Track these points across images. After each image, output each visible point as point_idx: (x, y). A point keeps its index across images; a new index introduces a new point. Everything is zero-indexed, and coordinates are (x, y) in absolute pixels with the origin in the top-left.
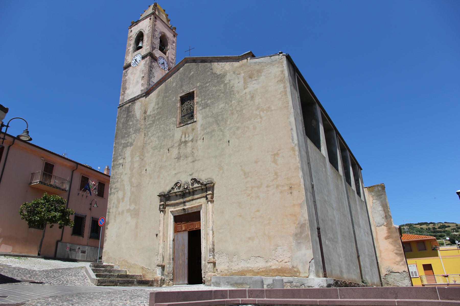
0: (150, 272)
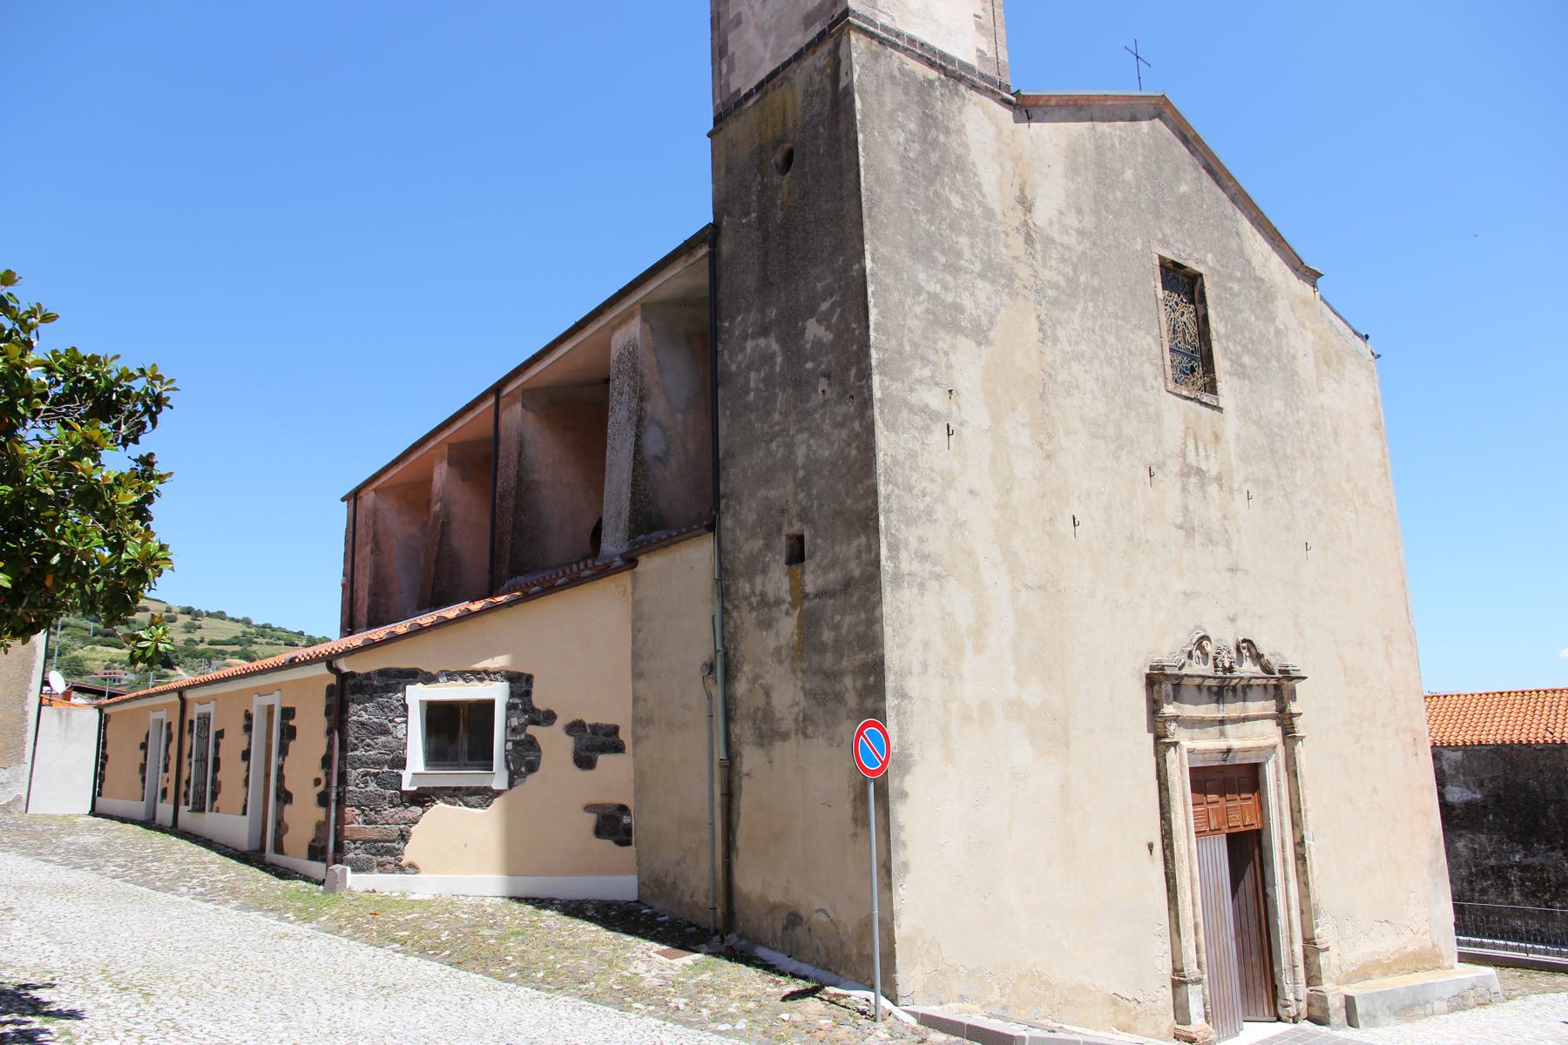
0: (1145, 1011)
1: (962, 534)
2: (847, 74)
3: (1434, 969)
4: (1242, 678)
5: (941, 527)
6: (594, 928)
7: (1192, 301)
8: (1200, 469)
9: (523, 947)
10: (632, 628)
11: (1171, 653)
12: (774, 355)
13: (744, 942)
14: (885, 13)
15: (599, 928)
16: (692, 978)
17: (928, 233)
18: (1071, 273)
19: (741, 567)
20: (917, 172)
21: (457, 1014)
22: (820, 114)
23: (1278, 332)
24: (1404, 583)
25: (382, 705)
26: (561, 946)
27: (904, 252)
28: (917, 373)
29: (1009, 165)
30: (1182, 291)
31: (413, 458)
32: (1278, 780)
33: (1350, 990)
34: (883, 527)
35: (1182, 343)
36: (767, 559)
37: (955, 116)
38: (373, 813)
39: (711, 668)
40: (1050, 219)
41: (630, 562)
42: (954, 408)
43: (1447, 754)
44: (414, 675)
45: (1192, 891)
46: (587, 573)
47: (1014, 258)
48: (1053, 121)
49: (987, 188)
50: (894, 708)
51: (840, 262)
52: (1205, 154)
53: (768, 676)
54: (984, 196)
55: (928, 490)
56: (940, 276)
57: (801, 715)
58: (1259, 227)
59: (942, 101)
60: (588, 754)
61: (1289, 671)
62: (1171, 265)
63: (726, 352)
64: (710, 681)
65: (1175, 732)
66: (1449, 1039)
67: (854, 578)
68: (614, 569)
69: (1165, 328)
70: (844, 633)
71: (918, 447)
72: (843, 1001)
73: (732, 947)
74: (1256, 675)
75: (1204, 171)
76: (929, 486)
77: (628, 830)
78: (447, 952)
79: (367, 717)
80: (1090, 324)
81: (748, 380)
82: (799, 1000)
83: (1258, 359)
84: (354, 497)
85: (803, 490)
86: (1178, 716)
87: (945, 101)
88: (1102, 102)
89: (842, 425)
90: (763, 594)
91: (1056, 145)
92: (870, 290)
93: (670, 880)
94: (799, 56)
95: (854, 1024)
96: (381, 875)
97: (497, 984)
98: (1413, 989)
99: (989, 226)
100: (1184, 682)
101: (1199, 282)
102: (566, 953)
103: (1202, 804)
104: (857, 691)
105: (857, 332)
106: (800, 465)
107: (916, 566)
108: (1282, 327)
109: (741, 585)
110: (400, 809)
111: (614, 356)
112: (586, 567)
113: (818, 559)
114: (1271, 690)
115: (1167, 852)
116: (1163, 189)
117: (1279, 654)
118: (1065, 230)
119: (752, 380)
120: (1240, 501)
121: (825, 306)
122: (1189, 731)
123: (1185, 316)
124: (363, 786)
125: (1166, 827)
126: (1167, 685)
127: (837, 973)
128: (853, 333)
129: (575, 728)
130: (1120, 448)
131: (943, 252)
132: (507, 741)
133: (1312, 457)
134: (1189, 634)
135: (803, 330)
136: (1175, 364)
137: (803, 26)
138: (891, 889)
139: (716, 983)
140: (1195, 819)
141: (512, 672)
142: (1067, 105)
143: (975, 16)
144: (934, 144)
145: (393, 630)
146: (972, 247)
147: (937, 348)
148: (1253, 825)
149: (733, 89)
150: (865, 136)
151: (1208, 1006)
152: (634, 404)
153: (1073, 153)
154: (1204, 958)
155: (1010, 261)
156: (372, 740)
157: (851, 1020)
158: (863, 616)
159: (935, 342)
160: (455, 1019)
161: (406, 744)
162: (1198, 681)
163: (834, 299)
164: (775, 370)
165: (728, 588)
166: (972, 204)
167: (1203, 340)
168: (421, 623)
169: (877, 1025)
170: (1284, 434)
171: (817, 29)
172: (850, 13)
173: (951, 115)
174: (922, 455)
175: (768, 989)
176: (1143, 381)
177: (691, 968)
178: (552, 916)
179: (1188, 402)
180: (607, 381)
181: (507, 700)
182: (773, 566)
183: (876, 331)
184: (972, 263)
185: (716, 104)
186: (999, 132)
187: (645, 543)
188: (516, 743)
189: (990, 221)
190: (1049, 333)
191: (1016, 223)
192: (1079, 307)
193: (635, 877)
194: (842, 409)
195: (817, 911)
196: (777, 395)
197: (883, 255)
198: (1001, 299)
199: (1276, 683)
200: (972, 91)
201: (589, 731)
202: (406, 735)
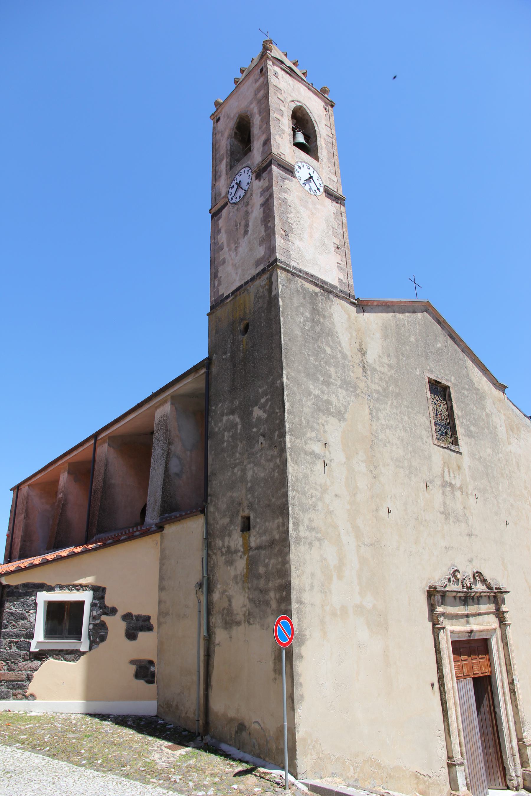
0: (434, 782)
1: (332, 517)
2: (275, 289)
4: (476, 592)
5: (321, 513)
6: (132, 732)
7: (445, 400)
9: (91, 744)
12: (237, 424)
13: (214, 740)
14: (295, 261)
15: (135, 732)
17: (314, 365)
18: (385, 386)
19: (218, 532)
21: (50, 788)
22: (262, 307)
23: (487, 415)
25: (23, 603)
26: (112, 743)
27: (302, 375)
28: (308, 435)
29: (354, 334)
30: (440, 395)
31: (50, 469)
32: (498, 647)
34: (291, 513)
35: (441, 420)
36: (231, 528)
37: (328, 309)
38: (13, 664)
39: (200, 585)
41: (160, 528)
42: (327, 452)
44: (42, 587)
45: (456, 710)
46: (138, 533)
47: (357, 378)
49: (343, 344)
50: (296, 609)
51: (271, 379)
52: (449, 329)
53: (230, 591)
54: (342, 348)
55: (314, 495)
56: (320, 387)
57: (247, 612)
58: (476, 363)
59: (322, 303)
60: (133, 631)
61: (501, 588)
62: (434, 382)
63: (213, 421)
64: (200, 593)
65: (444, 622)
67: (276, 540)
68: (152, 531)
69: (432, 413)
70: (270, 569)
71: (309, 472)
72: (267, 777)
73: (207, 743)
74: (484, 591)
75: (449, 337)
76: (315, 492)
77: (153, 675)
78: (48, 748)
79: (14, 609)
80: (395, 411)
81: (223, 436)
82: (243, 776)
83: (479, 429)
84: (17, 489)
85: (250, 493)
86: (444, 613)
87: (323, 302)
88: (399, 304)
89: (271, 460)
90: (229, 547)
92: (286, 393)
93: (175, 704)
94: (253, 279)
95: (274, 791)
96: (14, 701)
97: (74, 768)
99: (344, 362)
101: (448, 390)
102: (115, 748)
103: (459, 661)
104: (276, 599)
105: (279, 414)
106: (249, 480)
107: (307, 534)
108: (489, 412)
109: (217, 542)
110: (28, 662)
111: (156, 421)
112: (137, 530)
113: (257, 529)
114: (492, 598)
116: (429, 346)
117: (495, 579)
118: (382, 364)
119: (225, 436)
120: (472, 499)
121: (263, 401)
122: (450, 621)
123: (442, 407)
124: (9, 649)
125: (440, 674)
126: (438, 596)
127: (264, 760)
128: (277, 414)
129: (127, 617)
130: (411, 472)
131: (322, 375)
132: (90, 624)
133: (507, 477)
134: (449, 569)
135: (252, 412)
136: (437, 430)
137: (255, 266)
138: (294, 710)
139: (197, 766)
140: (455, 670)
141: (95, 586)
142: (382, 305)
143: (338, 263)
144: (318, 323)
145: (32, 562)
146: (336, 373)
147: (319, 422)
148: (486, 672)
149: (220, 293)
150: (284, 318)
151: (468, 780)
152: (165, 446)
153: (385, 328)
154: (464, 750)
155: (355, 379)
156: (16, 622)
157: (272, 788)
159: (318, 419)
160: (48, 791)
161: (35, 625)
162: (454, 594)
163: (267, 397)
164: (237, 432)
165: (210, 543)
167: (451, 418)
168: (48, 558)
170: (493, 465)
171: (261, 267)
175: (226, 769)
176: (422, 439)
178: (108, 725)
179: (444, 449)
180: (152, 433)
181: (92, 601)
182: (234, 532)
183: (288, 413)
184: (336, 380)
185: (211, 300)
186: (349, 318)
187: (168, 518)
188: (95, 625)
189: (345, 360)
190: (374, 415)
191: (358, 361)
192: (389, 403)
194: (270, 453)
195: (254, 723)
196: (238, 444)
197: (292, 376)
198: (351, 398)
199: (494, 594)
200: (336, 298)
201: (134, 618)
202: (35, 620)
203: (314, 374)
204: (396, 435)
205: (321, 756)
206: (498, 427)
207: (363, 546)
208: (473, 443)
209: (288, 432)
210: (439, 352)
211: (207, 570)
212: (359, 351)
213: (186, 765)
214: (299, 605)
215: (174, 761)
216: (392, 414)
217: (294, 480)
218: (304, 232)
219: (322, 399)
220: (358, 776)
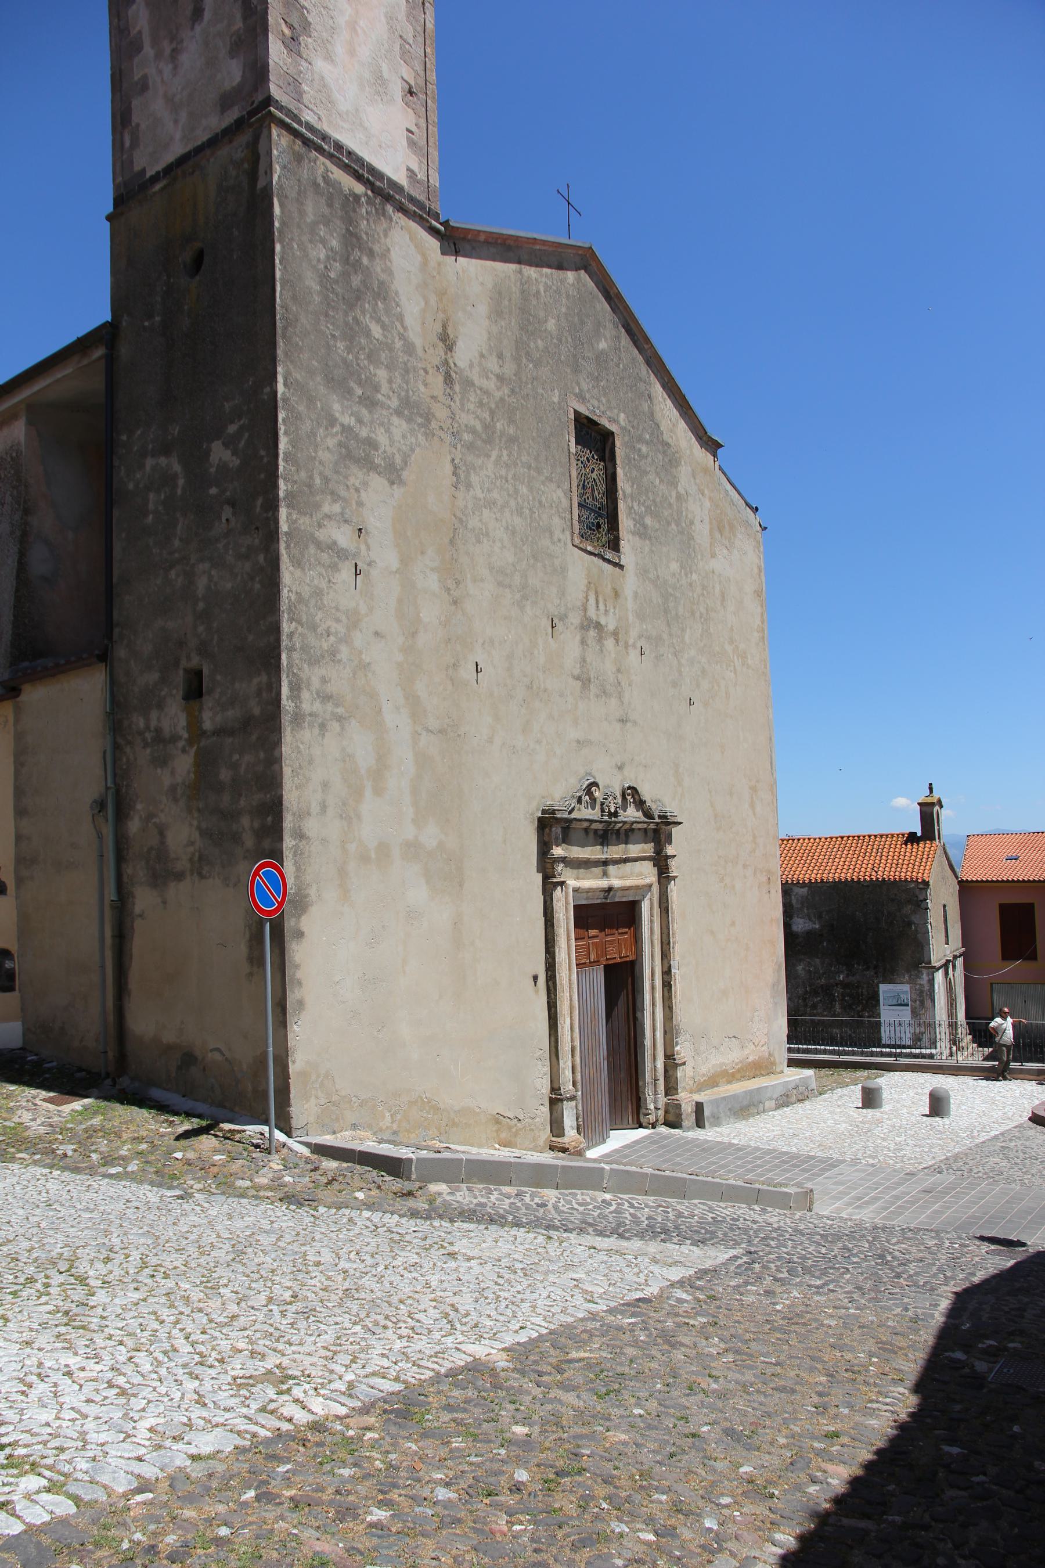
1: (366, 676)
2: (266, 173)
3: (768, 1074)
4: (625, 823)
5: (344, 668)
7: (602, 459)
8: (599, 623)
10: (15, 762)
11: (562, 798)
12: (175, 476)
14: (312, 110)
16: (81, 1123)
17: (345, 361)
18: (488, 419)
20: (337, 295)
23: (679, 497)
24: (771, 739)
27: (319, 379)
28: (326, 508)
29: (433, 299)
32: (652, 915)
33: (698, 1097)
34: (285, 664)
35: (591, 499)
36: (163, 693)
37: (380, 237)
39: (100, 805)
40: (471, 361)
42: (363, 547)
43: (797, 890)
47: (432, 397)
48: (481, 259)
49: (409, 321)
50: (292, 848)
52: (625, 314)
54: (405, 328)
55: (333, 630)
56: (355, 409)
57: (197, 854)
59: (368, 220)
63: (122, 468)
66: (773, 1131)
69: (575, 483)
71: (324, 585)
72: (237, 1137)
74: (638, 820)
76: (334, 626)
77: (11, 975)
80: (503, 472)
82: (193, 1139)
83: (659, 522)
87: (371, 221)
88: (531, 246)
90: (158, 731)
91: (482, 284)
92: (281, 415)
94: (214, 142)
98: (750, 1092)
99: (408, 360)
100: (573, 826)
103: (584, 938)
105: (265, 460)
106: (200, 596)
107: (317, 706)
108: (683, 492)
113: (217, 696)
114: (650, 834)
115: (550, 983)
116: (583, 344)
118: (485, 373)
120: (633, 655)
121: (232, 429)
122: (575, 871)
125: (550, 960)
127: (232, 1110)
130: (525, 597)
131: (360, 383)
133: (701, 617)
134: (580, 781)
135: (208, 453)
138: (285, 1027)
144: (357, 266)
146: (390, 381)
147: (348, 483)
149: (137, 168)
150: (283, 247)
151: (580, 1120)
153: (498, 294)
155: (428, 400)
157: (245, 1154)
158: (262, 755)
159: (346, 477)
162: (585, 824)
163: (242, 422)
166: (392, 336)
169: (271, 1157)
170: (678, 595)
171: (233, 115)
172: (272, 103)
173: (376, 236)
174: (328, 593)
175: (161, 1130)
176: (551, 534)
177: (80, 1113)
179: (593, 557)
183: (285, 460)
184: (389, 398)
187: (29, 671)
189: (411, 356)
190: (462, 477)
191: (437, 361)
192: (494, 454)
193: (20, 1023)
195: (212, 1050)
197: (296, 380)
198: (417, 439)
200: (400, 215)
203: (345, 379)
204: (501, 521)
205: (335, 1098)
206: (695, 522)
207: (424, 733)
208: (647, 549)
209: (284, 499)
210: (600, 359)
211: (115, 775)
212: (441, 340)
213: (84, 1126)
214: (297, 841)
215: (60, 1122)
216: (496, 478)
217: (293, 598)
218: (335, 37)
219: (357, 435)
220: (399, 1127)
